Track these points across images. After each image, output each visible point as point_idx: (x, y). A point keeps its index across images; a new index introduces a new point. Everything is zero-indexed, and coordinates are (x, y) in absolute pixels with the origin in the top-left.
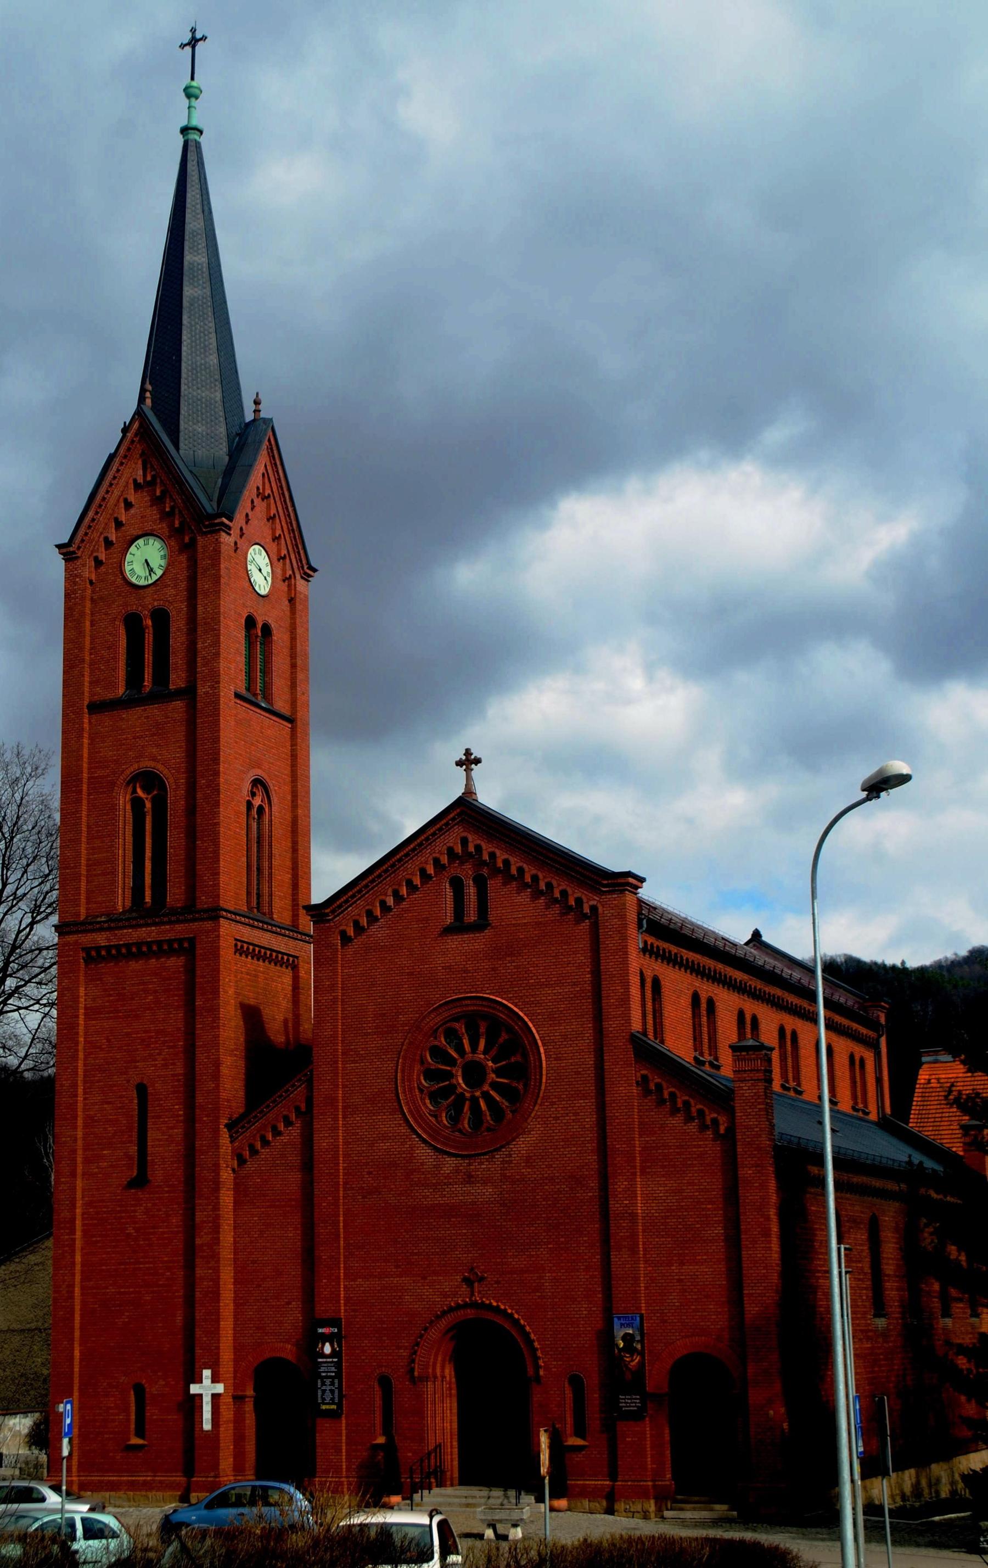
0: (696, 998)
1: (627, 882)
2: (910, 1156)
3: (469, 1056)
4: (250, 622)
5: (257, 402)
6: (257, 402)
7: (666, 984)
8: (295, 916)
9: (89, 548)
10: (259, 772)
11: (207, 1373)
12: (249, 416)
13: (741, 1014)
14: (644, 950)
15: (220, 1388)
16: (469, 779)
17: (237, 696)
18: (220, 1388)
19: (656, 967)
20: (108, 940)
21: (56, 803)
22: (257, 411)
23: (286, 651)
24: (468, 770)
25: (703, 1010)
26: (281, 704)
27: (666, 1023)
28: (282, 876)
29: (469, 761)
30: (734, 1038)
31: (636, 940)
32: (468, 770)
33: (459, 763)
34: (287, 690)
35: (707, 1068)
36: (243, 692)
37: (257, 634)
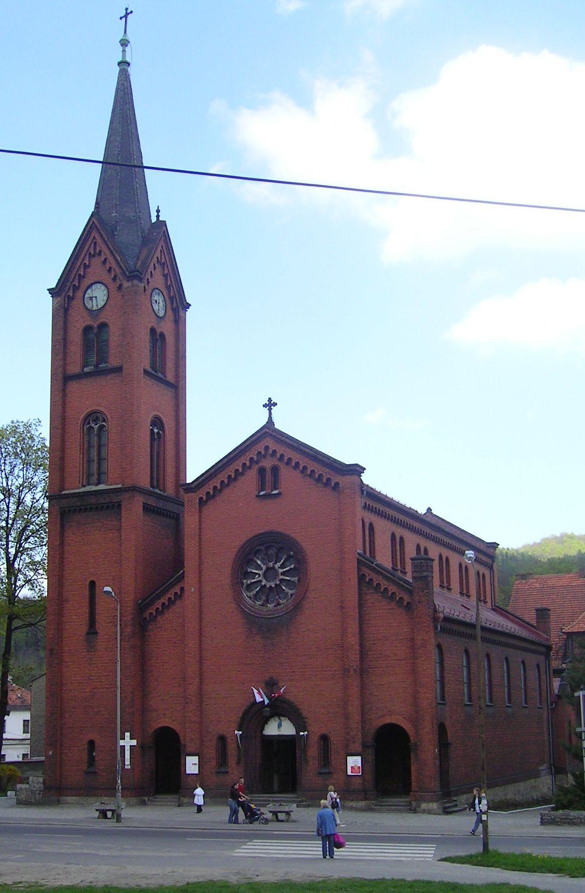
0: (393, 536)
1: (357, 470)
2: (392, 142)
3: (277, 566)
4: (153, 331)
5: (158, 211)
6: (158, 211)
7: (377, 528)
8: (177, 492)
9: (66, 292)
10: (156, 413)
11: (127, 734)
12: (154, 220)
13: (418, 546)
14: (365, 507)
15: (134, 742)
16: (270, 414)
17: (146, 372)
18: (134, 742)
19: (370, 517)
20: (534, 788)
21: (48, 437)
22: (158, 216)
23: (173, 349)
24: (270, 410)
25: (397, 543)
26: (170, 377)
27: (377, 548)
28: (170, 470)
29: (270, 405)
30: (414, 555)
31: (360, 501)
32: (270, 410)
33: (265, 406)
34: (173, 369)
35: (399, 573)
36: (150, 370)
37: (157, 337)
